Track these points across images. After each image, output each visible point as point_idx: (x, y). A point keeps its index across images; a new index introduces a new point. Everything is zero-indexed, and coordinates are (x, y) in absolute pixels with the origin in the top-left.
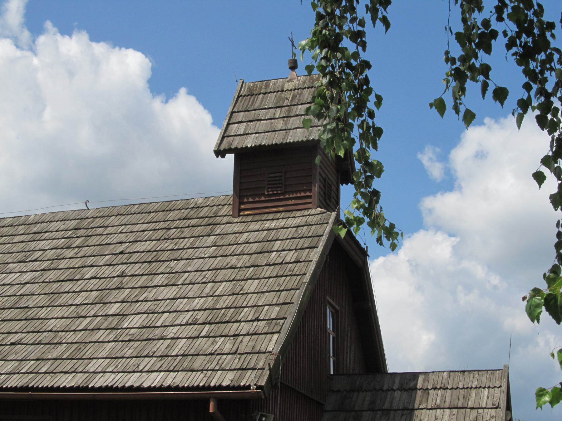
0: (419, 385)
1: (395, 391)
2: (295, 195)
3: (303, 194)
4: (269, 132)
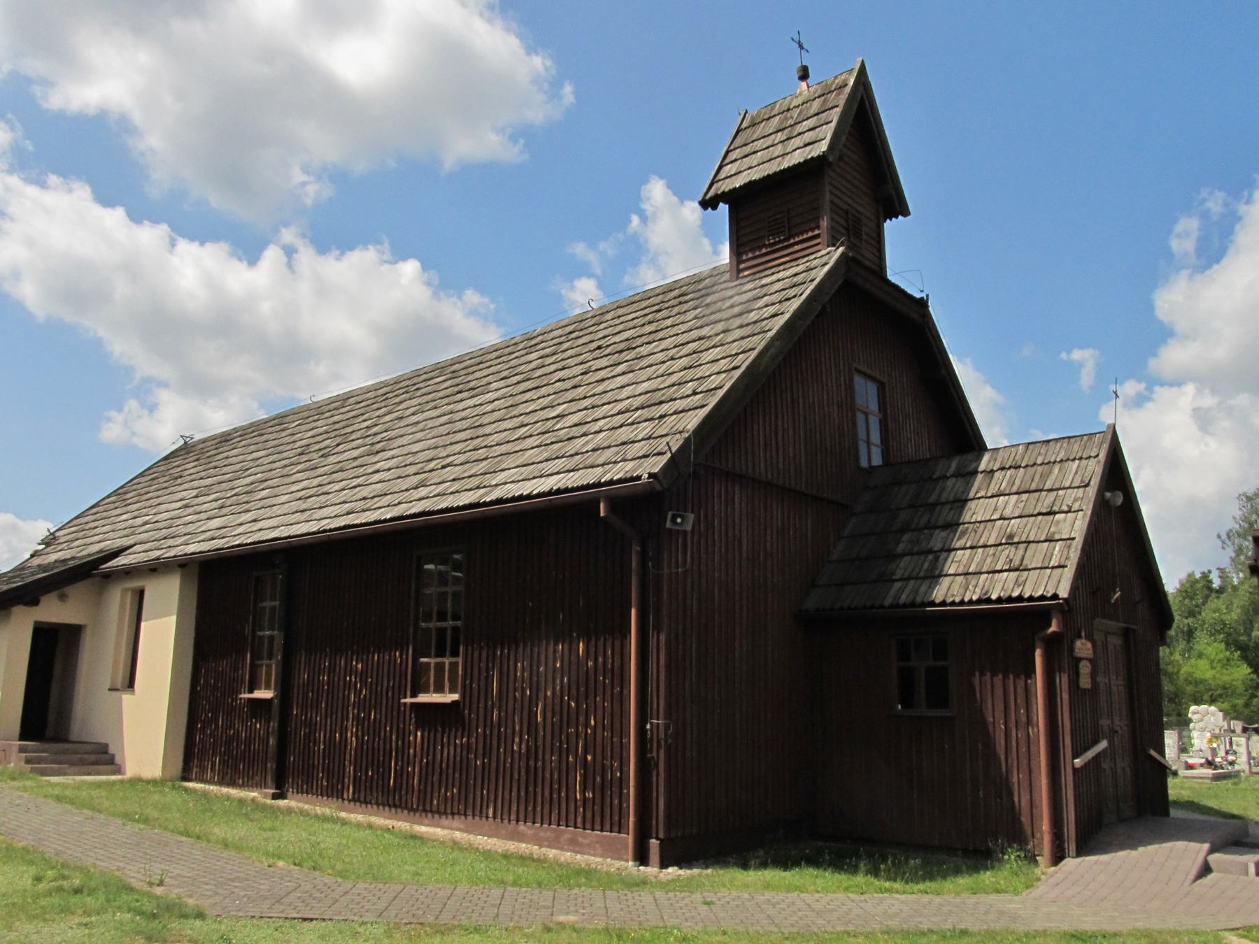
0: (982, 467)
1: (948, 478)
2: (801, 238)
3: (810, 234)
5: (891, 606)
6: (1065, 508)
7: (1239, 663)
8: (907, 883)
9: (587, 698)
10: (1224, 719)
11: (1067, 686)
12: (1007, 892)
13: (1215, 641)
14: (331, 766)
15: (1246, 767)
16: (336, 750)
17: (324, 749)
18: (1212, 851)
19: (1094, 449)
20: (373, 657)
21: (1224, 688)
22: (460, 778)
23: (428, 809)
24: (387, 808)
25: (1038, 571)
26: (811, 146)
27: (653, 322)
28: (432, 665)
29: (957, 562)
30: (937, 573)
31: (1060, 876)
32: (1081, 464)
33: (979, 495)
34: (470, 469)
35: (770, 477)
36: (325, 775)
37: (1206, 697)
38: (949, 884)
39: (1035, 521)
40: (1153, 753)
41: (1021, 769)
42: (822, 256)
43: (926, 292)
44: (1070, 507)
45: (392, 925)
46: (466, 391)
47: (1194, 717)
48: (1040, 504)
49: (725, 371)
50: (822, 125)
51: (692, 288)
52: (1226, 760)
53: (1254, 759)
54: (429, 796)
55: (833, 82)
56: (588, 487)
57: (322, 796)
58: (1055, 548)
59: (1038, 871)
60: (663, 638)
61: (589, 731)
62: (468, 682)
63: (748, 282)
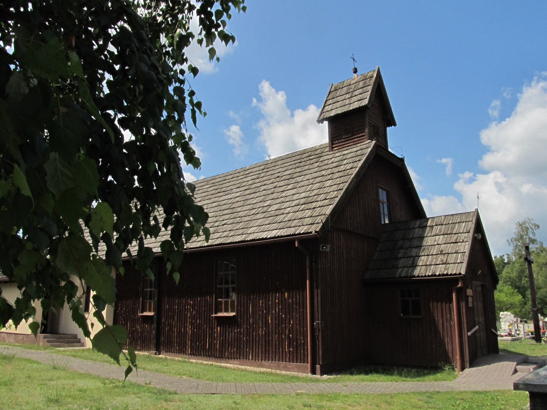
0: (429, 224)
1: (416, 228)
2: (357, 136)
3: (361, 135)
4: (342, 107)
5: (399, 277)
6: (461, 241)
7: (517, 294)
8: (412, 378)
9: (289, 313)
10: (515, 317)
12: (447, 380)
13: (506, 285)
14: (180, 341)
15: (523, 336)
16: (182, 335)
17: (177, 335)
18: (517, 365)
20: (198, 299)
21: (511, 304)
22: (237, 345)
23: (224, 357)
24: (205, 357)
25: (453, 264)
26: (361, 101)
27: (299, 167)
28: (223, 302)
30: (415, 265)
31: (464, 375)
33: (428, 235)
34: (236, 226)
35: (352, 229)
36: (178, 344)
37: (504, 309)
38: (426, 378)
39: (450, 245)
40: (493, 330)
42: (366, 144)
43: (404, 155)
44: (463, 240)
45: (243, 395)
46: (222, 192)
47: (502, 317)
48: (452, 239)
49: (336, 191)
50: (365, 92)
51: (313, 153)
52: (516, 333)
53: (526, 333)
54: (224, 352)
55: (367, 75)
56: (290, 235)
57: (176, 353)
59: (456, 373)
60: (319, 291)
61: (290, 326)
62: (239, 308)
63: (337, 152)
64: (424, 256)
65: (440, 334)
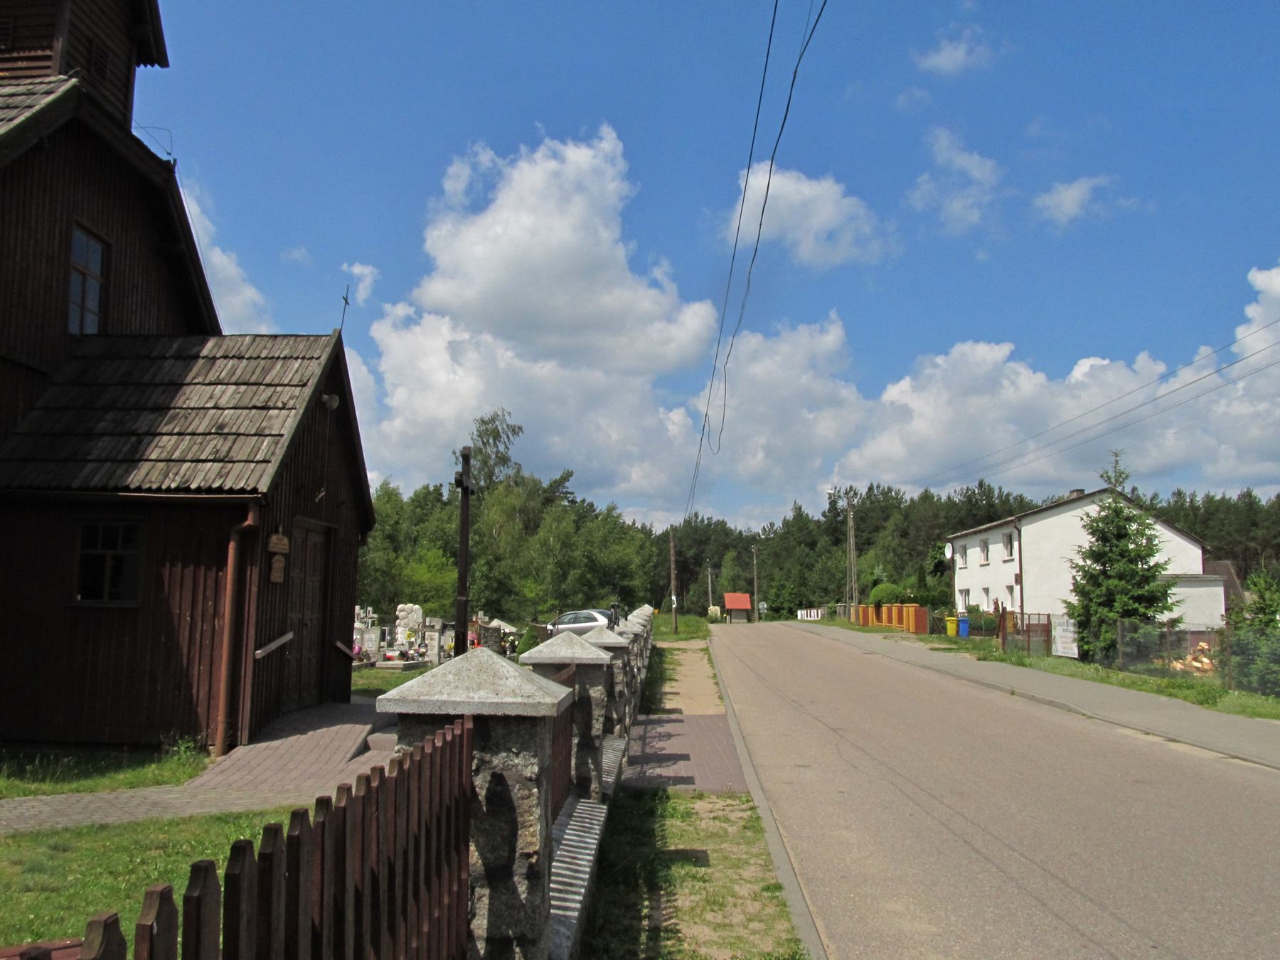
0: (205, 352)
1: (167, 358)
2: (27, 54)
3: (40, 53)
5: (80, 489)
6: (280, 405)
8: (57, 782)
11: (257, 579)
19: (318, 351)
25: (243, 464)
29: (160, 447)
30: (137, 456)
31: (228, 763)
32: (303, 364)
33: (196, 381)
40: (339, 644)
41: (202, 662)
43: (175, 155)
48: (256, 398)
58: (263, 442)
64: (171, 434)
65: (182, 655)
